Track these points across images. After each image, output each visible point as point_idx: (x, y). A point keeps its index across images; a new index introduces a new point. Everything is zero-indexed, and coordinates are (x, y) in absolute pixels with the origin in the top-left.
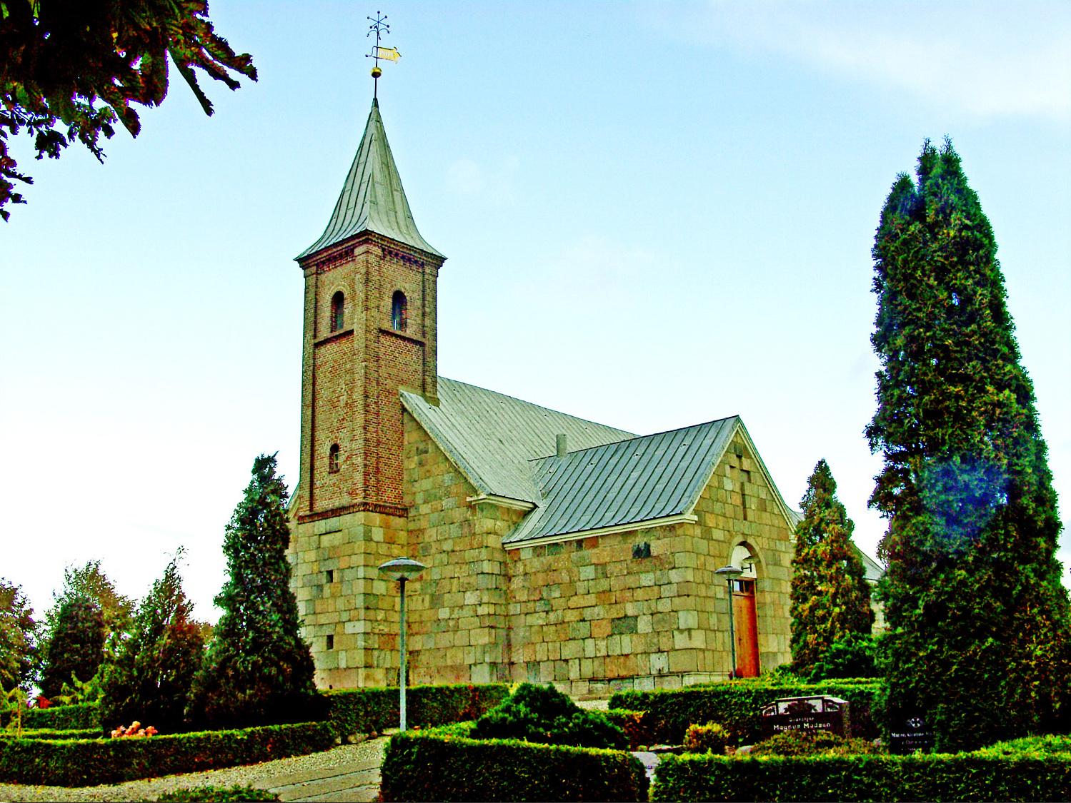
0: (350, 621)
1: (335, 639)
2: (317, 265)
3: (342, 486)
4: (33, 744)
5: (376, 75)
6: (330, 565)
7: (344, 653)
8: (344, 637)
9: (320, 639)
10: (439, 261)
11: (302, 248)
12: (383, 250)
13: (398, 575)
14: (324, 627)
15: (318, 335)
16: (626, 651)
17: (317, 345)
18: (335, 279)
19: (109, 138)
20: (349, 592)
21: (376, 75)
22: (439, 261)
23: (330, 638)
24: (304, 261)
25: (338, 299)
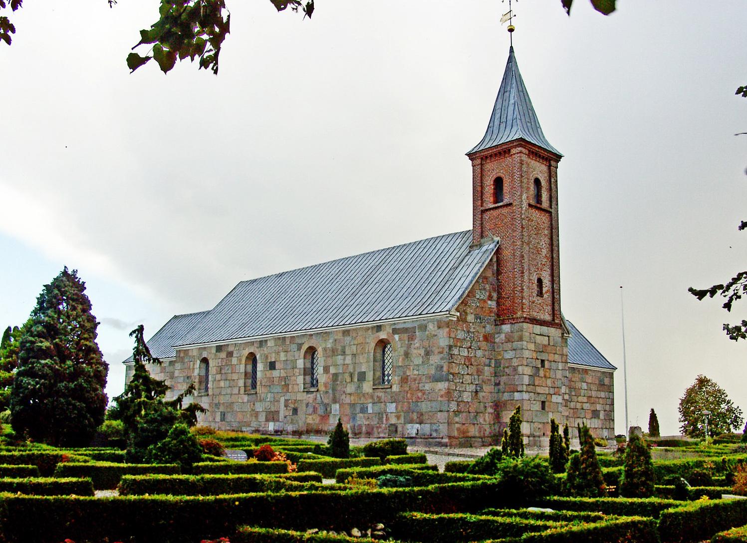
0: (554, 394)
1: (547, 404)
2: (482, 159)
3: (545, 308)
4: (99, 454)
5: (511, 30)
6: (544, 356)
7: (551, 413)
8: (551, 403)
9: (538, 403)
10: (558, 157)
11: (469, 149)
12: (529, 151)
13: (246, 352)
14: (540, 395)
15: (484, 204)
16: (596, 427)
17: (483, 212)
18: (494, 169)
19: (14, 11)
20: (554, 376)
21: (511, 30)
22: (558, 157)
23: (543, 403)
24: (471, 155)
25: (499, 182)
